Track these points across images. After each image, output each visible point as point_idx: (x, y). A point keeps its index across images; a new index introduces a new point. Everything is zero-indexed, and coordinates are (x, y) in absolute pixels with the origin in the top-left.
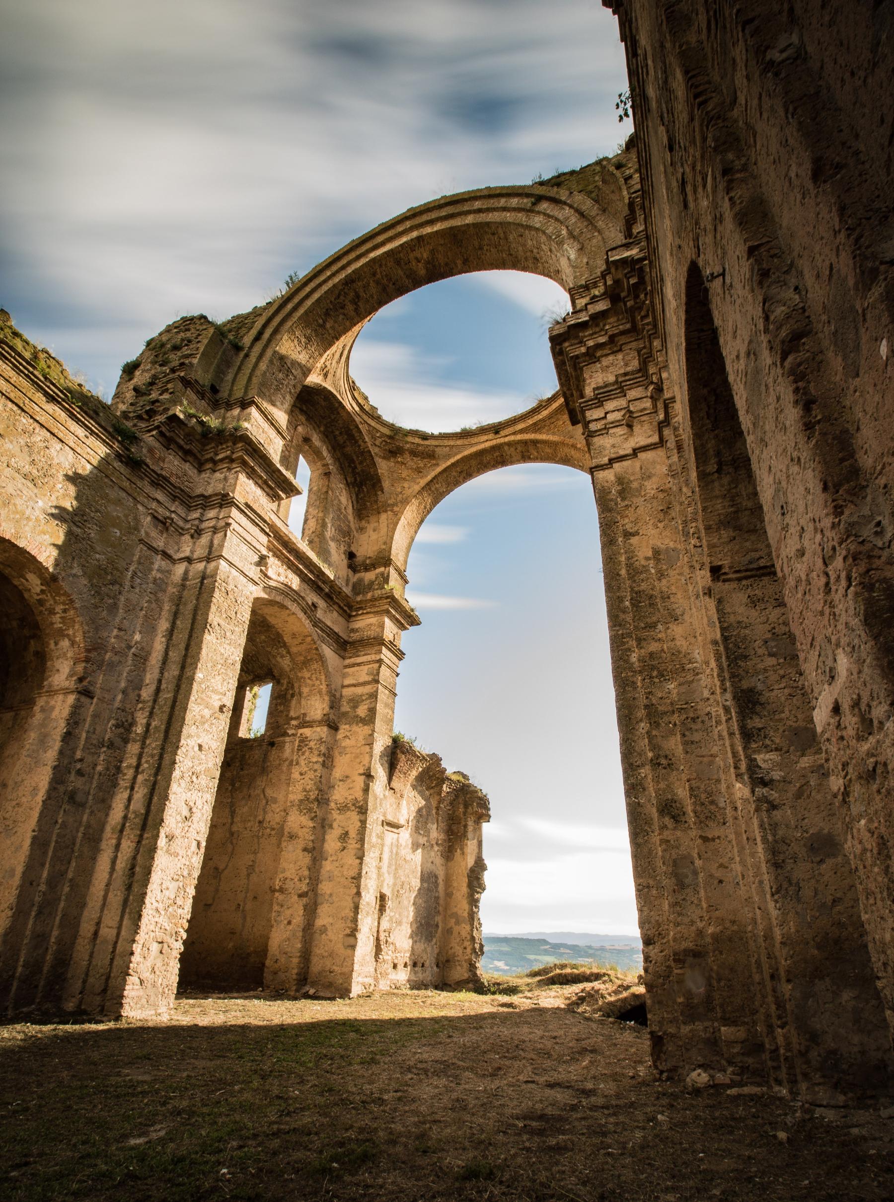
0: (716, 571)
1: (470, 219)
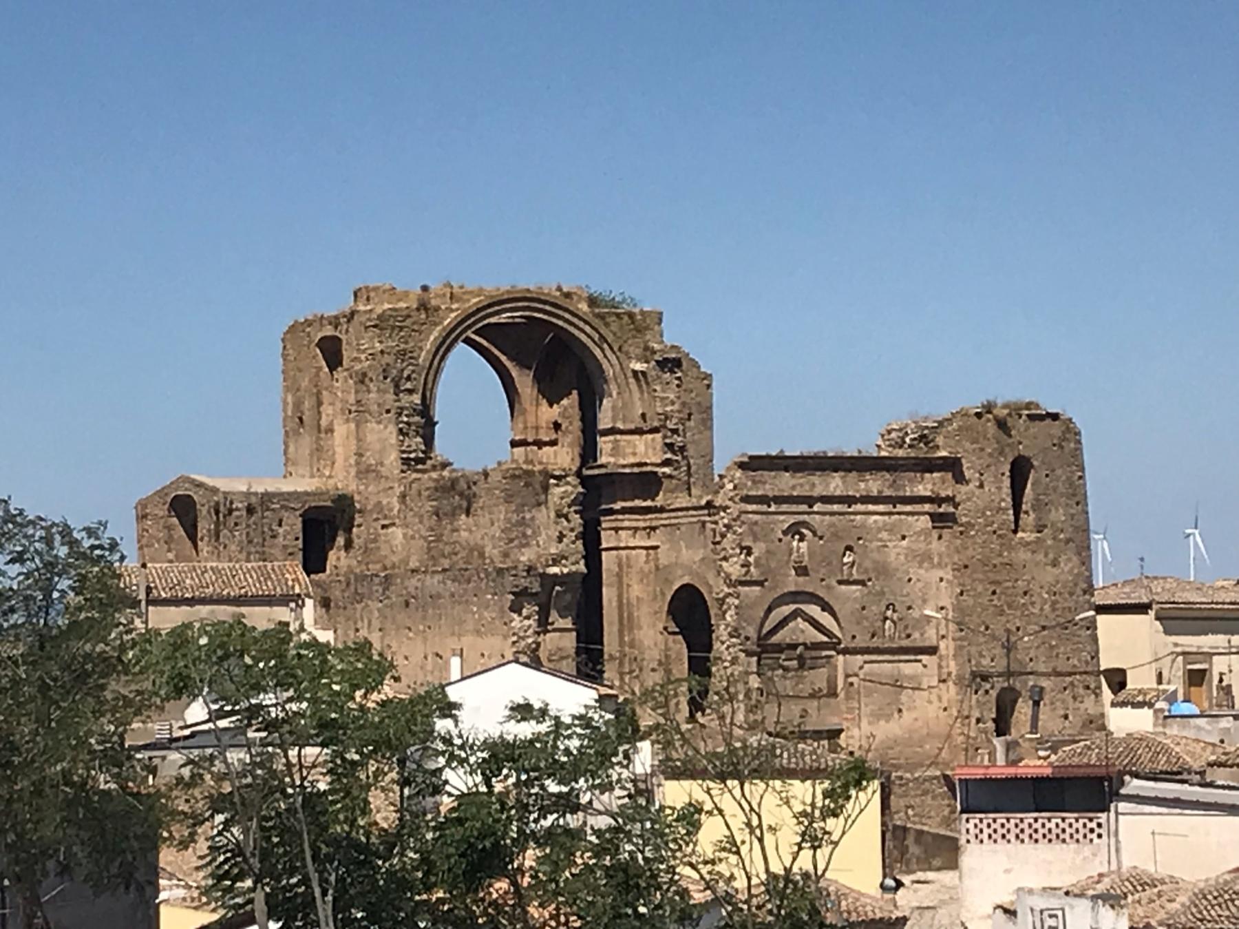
0: (665, 628)
1: (560, 323)
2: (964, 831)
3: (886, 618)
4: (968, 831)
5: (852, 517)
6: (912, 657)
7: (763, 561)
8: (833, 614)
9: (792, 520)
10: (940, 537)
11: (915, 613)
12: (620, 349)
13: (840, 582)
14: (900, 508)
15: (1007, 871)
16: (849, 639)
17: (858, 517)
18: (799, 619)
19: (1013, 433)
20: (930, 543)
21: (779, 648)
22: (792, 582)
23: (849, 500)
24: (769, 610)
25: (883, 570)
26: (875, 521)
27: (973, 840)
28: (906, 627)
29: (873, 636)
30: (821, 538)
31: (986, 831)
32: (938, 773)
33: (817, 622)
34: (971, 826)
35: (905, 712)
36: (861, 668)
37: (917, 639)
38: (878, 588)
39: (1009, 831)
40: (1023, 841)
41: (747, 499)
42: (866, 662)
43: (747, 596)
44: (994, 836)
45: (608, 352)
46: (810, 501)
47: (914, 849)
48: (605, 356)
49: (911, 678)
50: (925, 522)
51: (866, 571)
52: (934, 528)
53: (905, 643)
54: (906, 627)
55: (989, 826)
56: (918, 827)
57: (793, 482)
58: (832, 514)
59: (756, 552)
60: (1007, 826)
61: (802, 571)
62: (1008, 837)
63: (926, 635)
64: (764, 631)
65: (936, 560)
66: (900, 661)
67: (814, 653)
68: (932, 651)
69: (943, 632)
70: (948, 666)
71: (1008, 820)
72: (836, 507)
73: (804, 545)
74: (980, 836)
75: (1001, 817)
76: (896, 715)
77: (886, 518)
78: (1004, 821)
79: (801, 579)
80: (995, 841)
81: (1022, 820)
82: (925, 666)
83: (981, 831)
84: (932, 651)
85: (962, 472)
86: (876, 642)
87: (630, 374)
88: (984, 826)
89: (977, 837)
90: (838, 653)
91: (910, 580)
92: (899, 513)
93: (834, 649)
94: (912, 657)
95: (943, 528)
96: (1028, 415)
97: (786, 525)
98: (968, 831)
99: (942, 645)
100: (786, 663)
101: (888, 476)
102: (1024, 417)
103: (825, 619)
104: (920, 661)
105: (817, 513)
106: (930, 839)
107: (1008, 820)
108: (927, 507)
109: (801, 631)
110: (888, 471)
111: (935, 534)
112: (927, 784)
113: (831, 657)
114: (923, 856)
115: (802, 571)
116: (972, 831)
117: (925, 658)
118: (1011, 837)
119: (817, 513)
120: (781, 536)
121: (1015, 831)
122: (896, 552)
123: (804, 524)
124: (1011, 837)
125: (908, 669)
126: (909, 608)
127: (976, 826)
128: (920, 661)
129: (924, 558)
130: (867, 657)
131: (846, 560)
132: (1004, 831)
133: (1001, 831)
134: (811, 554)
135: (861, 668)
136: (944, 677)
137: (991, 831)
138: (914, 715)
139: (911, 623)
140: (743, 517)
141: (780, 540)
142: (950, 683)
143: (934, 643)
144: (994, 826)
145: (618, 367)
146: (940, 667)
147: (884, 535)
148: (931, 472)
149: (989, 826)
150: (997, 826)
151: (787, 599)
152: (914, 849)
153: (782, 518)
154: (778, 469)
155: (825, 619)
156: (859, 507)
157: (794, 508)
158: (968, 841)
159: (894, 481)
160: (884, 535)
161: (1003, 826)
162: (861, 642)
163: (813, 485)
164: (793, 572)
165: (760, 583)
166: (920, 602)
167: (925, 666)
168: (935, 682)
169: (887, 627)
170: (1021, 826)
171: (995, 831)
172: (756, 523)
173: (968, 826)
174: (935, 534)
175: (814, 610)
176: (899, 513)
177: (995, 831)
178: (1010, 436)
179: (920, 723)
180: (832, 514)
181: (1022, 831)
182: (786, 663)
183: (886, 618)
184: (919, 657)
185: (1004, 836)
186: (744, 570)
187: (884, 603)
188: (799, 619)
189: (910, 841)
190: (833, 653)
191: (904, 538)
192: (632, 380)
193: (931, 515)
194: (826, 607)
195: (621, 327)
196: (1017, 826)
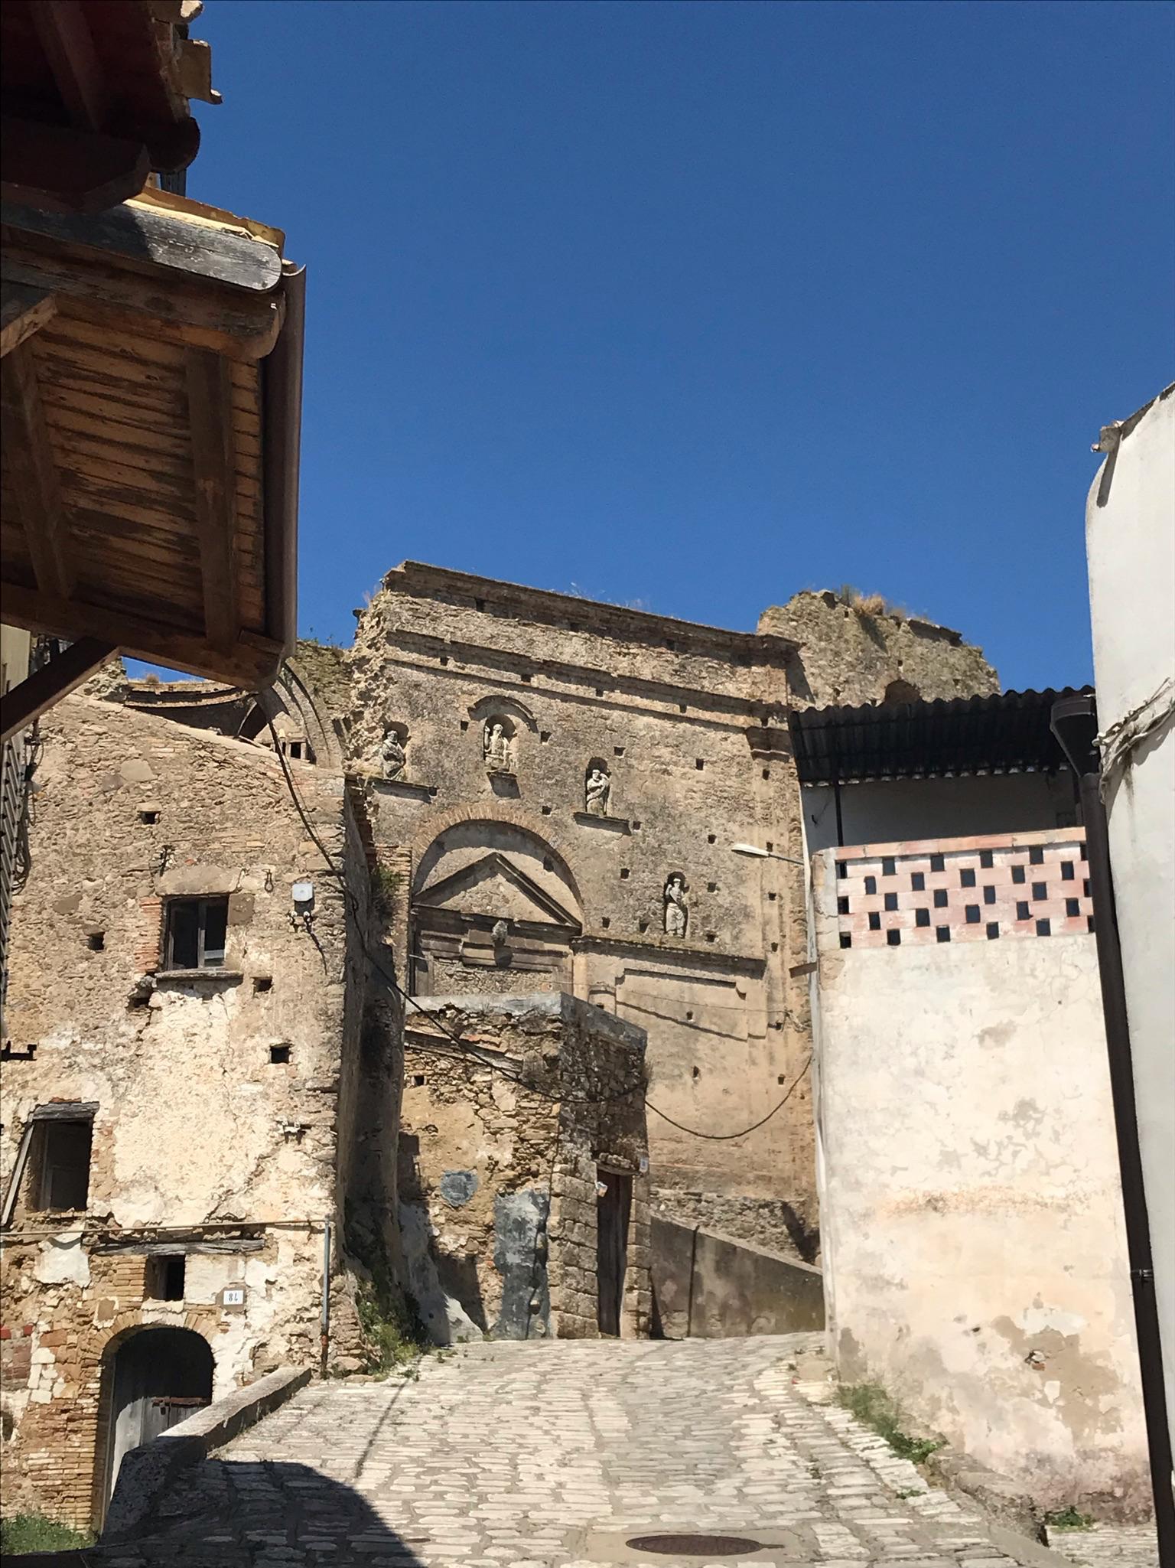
2: (830, 905)
3: (668, 899)
4: (843, 905)
5: (605, 712)
6: (717, 976)
7: (429, 754)
8: (566, 875)
9: (488, 691)
10: (766, 775)
11: (723, 898)
12: (316, 691)
13: (581, 818)
14: (692, 712)
15: (995, 1035)
16: (597, 925)
17: (616, 714)
18: (500, 878)
19: (888, 643)
20: (748, 781)
21: (461, 922)
22: (487, 805)
23: (597, 679)
24: (439, 847)
25: (663, 813)
26: (648, 727)
27: (861, 933)
28: (706, 919)
29: (643, 927)
30: (545, 736)
31: (910, 901)
32: (769, 1197)
33: (722, 1552)
34: (853, 887)
35: (705, 1078)
36: (620, 980)
37: (726, 942)
38: (651, 840)
39: (990, 894)
40: (1044, 928)
41: (399, 638)
42: (628, 971)
43: (392, 811)
44: (938, 916)
45: (299, 695)
46: (525, 666)
47: (715, 1287)
48: (294, 699)
49: (717, 1012)
50: (739, 744)
51: (630, 808)
52: (755, 755)
53: (704, 946)
54: (706, 919)
55: (918, 881)
56: (721, 1235)
57: (491, 630)
58: (566, 698)
59: (415, 738)
60: (983, 877)
61: (506, 783)
62: (988, 915)
63: (743, 940)
64: (431, 881)
65: (759, 812)
66: (698, 980)
67: (527, 943)
68: (756, 968)
69: (776, 938)
70: (785, 1000)
71: (987, 859)
72: (573, 689)
73: (513, 746)
74: (887, 921)
75: (961, 851)
76: (688, 1077)
77: (667, 724)
78: (974, 862)
79: (504, 801)
80: (943, 935)
81: (1036, 854)
82: (742, 996)
83: (891, 902)
84: (756, 968)
85: (803, 680)
86: (651, 937)
87: (329, 726)
88: (900, 883)
89: (875, 922)
90: (575, 951)
91: (712, 839)
92: (692, 721)
93: (568, 942)
94: (717, 976)
95: (769, 757)
96: (912, 624)
97: (476, 699)
98: (843, 905)
99: (774, 961)
100: (469, 952)
101: (670, 656)
102: (904, 626)
103: (552, 884)
104: (732, 985)
105: (536, 690)
106: (749, 1266)
107: (987, 859)
108: (741, 720)
109: (498, 897)
110: (670, 646)
111: (757, 767)
112: (750, 1216)
113: (560, 954)
114: (735, 1303)
115: (506, 783)
116: (861, 904)
117: (742, 981)
118: (1002, 913)
119: (536, 690)
120: (467, 719)
121: (1011, 893)
122: (684, 786)
123: (509, 701)
124: (1002, 913)
125: (712, 996)
126: (712, 887)
127: (870, 885)
128: (732, 985)
129: (739, 805)
130: (632, 963)
131: (591, 783)
132: (975, 896)
133: (961, 898)
134: (527, 762)
135: (620, 980)
136: (779, 1018)
137: (925, 900)
138: (722, 1084)
139: (716, 913)
140: (392, 671)
141: (464, 725)
142: (790, 1030)
143: (758, 954)
144: (934, 881)
145: (312, 715)
146: (770, 999)
147: (664, 752)
148: (748, 665)
149: (918, 881)
150: (948, 879)
151: (472, 834)
152: (715, 1287)
153: (467, 686)
154: (464, 604)
155: (552, 884)
156: (618, 697)
157: (494, 674)
158: (846, 941)
159: (683, 666)
160: (664, 752)
161: (968, 878)
162: (622, 929)
163: (531, 642)
164: (488, 786)
165: (425, 793)
166: (731, 879)
167: (742, 996)
168: (761, 1028)
169: (670, 912)
170: (1034, 875)
171: (941, 898)
172: (417, 686)
173: (848, 924)
174: (757, 767)
175: (530, 865)
176: (692, 721)
177: (941, 898)
178: (883, 647)
179: (732, 1100)
180: (566, 698)
181: (1040, 891)
182: (469, 952)
183: (668, 899)
184: (731, 978)
185: (972, 914)
186: (388, 766)
187: (664, 870)
188: (500, 878)
189: (705, 1266)
190: (565, 948)
191: (700, 765)
192: (332, 737)
193: (748, 732)
194: (553, 861)
195: (322, 665)
196: (1018, 875)
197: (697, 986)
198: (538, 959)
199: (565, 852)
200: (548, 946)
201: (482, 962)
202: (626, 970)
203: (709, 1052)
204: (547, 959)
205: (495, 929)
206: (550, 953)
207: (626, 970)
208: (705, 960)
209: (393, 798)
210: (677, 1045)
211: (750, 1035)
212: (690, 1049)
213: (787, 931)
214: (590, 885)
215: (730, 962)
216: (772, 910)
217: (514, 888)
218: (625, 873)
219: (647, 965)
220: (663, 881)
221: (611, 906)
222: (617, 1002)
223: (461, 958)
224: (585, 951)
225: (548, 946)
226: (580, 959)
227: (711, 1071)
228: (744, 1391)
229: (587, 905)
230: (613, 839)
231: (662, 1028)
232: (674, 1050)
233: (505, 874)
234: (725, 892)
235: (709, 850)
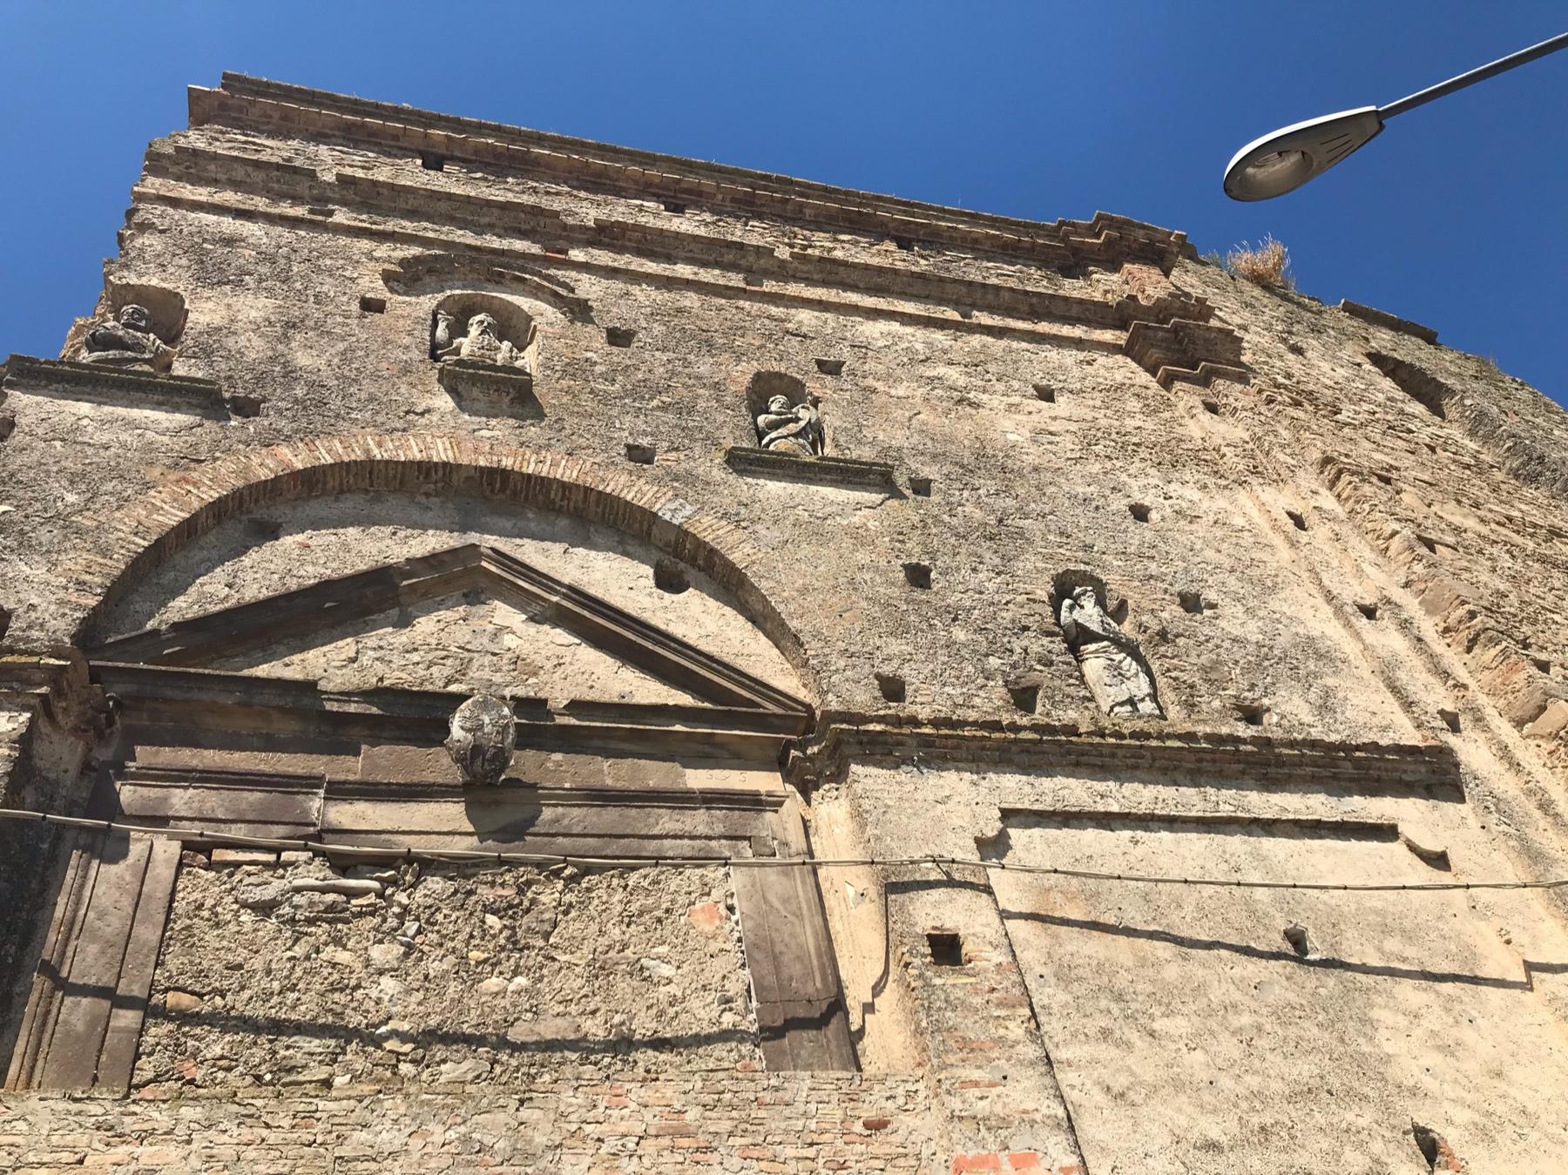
8: (731, 586)
11: (1234, 621)
13: (741, 462)
37: (1292, 711)
57: (711, 625)
93: (780, 763)
103: (698, 619)
104: (1386, 832)
113: (754, 802)
117: (1412, 814)
128: (1386, 832)
130: (1015, 788)
135: (994, 847)
155: (698, 619)
197: (1276, 847)
198: (666, 820)
199: (709, 529)
200: (699, 779)
201: (419, 845)
202: (1008, 815)
203: (1434, 1059)
204: (698, 820)
205: (457, 731)
206: (710, 799)
207: (1008, 815)
208: (1271, 764)
209: (85, 408)
210: (1301, 1048)
211: (1530, 967)
212: (1360, 1061)
213: (1462, 675)
214: (811, 601)
215: (1348, 768)
216: (1387, 638)
217: (561, 636)
218: (918, 576)
219: (1075, 791)
220: (1043, 591)
221: (895, 646)
222: (1005, 915)
223: (316, 838)
224: (840, 776)
225: (699, 779)
226: (831, 810)
227: (1483, 1135)
228: (341, 484)
229: (813, 648)
230: (858, 507)
231: (1216, 994)
232: (1305, 1069)
233: (518, 598)
234: (1230, 609)
235: (1138, 535)
